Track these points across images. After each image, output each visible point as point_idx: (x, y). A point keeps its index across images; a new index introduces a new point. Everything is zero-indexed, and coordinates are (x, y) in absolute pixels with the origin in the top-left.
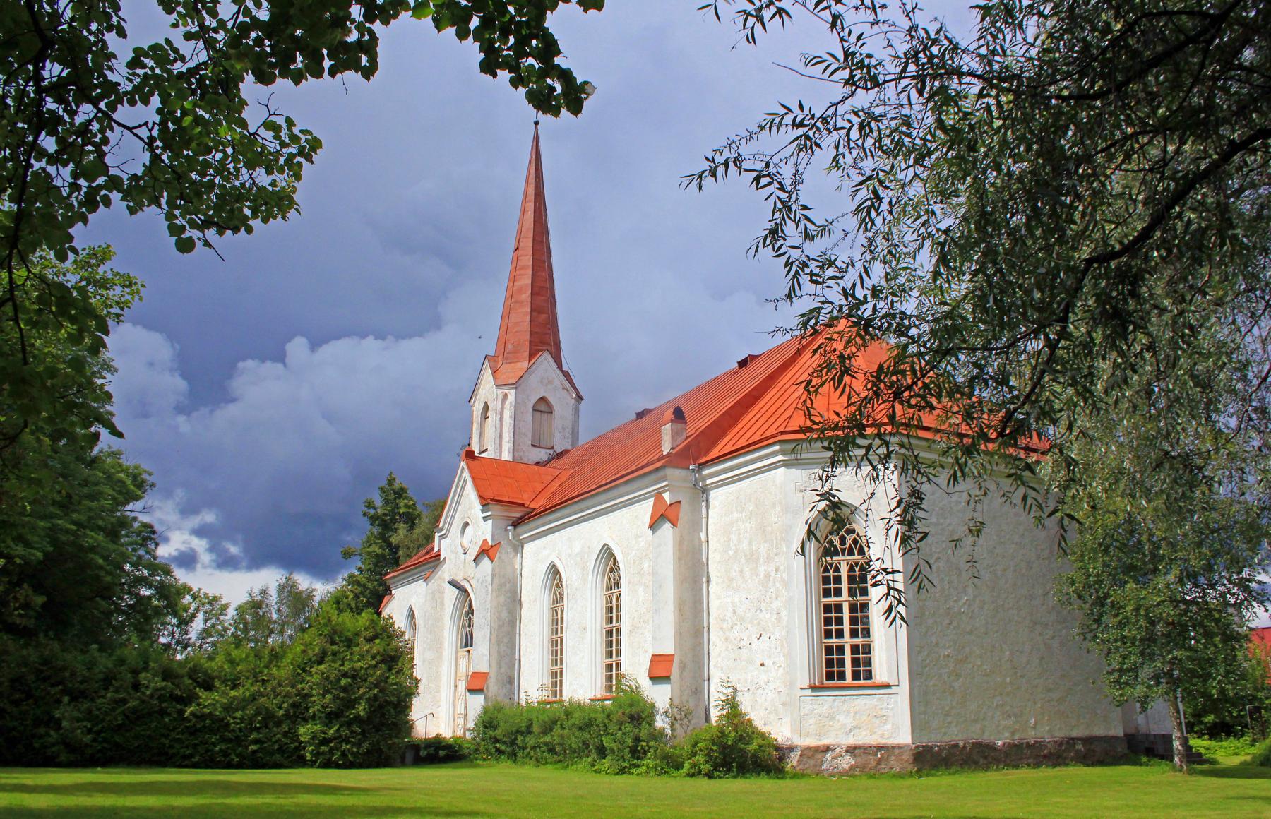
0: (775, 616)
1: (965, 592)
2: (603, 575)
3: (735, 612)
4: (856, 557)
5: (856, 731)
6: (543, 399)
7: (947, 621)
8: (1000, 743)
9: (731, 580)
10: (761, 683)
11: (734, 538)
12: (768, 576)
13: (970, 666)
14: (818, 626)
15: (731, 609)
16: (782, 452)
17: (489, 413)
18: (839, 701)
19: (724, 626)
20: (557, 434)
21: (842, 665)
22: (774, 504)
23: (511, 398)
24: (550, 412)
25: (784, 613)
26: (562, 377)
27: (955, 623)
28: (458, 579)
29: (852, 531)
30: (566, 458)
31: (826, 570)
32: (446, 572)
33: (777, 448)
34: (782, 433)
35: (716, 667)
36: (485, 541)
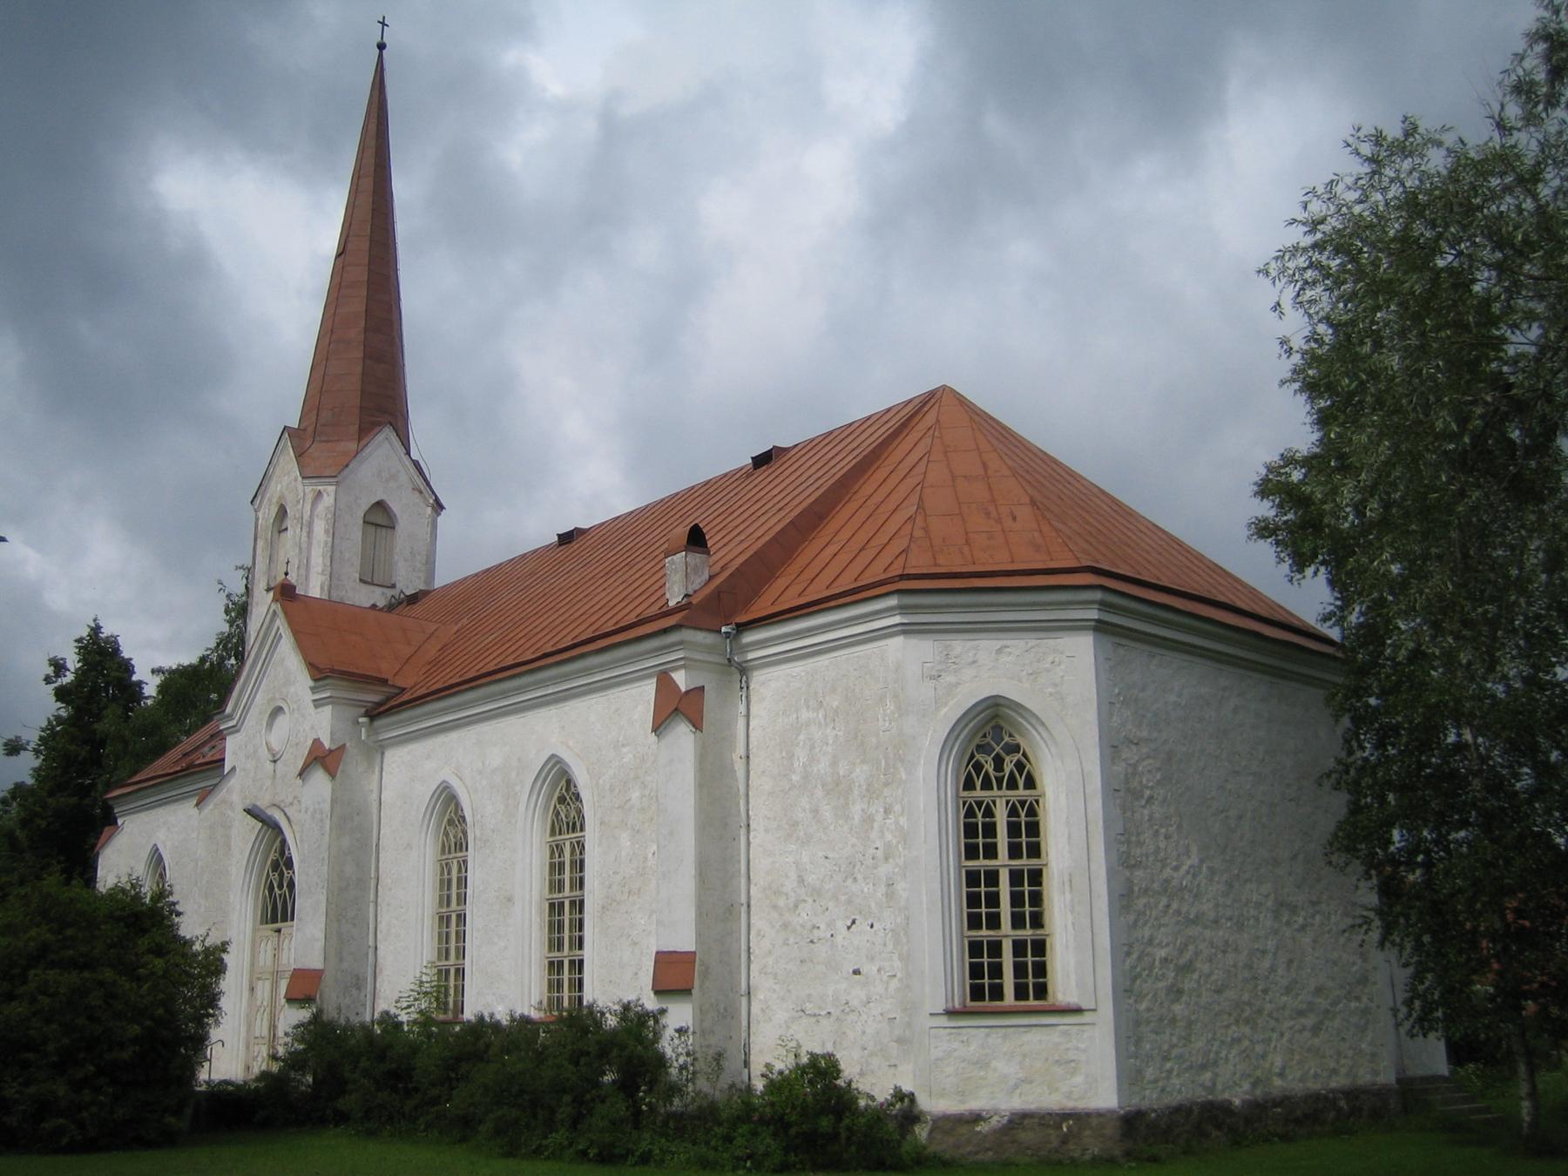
0: (882, 889)
1: (1188, 853)
2: (546, 808)
3: (801, 880)
4: (1021, 792)
6: (380, 506)
7: (1164, 901)
9: (795, 824)
10: (855, 1003)
11: (801, 755)
12: (868, 820)
13: (1196, 976)
14: (957, 909)
15: (793, 875)
16: (903, 609)
17: (288, 523)
18: (995, 1038)
19: (781, 902)
20: (401, 564)
21: (1001, 970)
23: (328, 500)
25: (901, 886)
26: (412, 469)
27: (1175, 905)
28: (263, 803)
29: (1016, 748)
30: (418, 608)
31: (970, 813)
32: (235, 792)
33: (893, 601)
34: (903, 577)
35: (763, 971)
36: (317, 743)
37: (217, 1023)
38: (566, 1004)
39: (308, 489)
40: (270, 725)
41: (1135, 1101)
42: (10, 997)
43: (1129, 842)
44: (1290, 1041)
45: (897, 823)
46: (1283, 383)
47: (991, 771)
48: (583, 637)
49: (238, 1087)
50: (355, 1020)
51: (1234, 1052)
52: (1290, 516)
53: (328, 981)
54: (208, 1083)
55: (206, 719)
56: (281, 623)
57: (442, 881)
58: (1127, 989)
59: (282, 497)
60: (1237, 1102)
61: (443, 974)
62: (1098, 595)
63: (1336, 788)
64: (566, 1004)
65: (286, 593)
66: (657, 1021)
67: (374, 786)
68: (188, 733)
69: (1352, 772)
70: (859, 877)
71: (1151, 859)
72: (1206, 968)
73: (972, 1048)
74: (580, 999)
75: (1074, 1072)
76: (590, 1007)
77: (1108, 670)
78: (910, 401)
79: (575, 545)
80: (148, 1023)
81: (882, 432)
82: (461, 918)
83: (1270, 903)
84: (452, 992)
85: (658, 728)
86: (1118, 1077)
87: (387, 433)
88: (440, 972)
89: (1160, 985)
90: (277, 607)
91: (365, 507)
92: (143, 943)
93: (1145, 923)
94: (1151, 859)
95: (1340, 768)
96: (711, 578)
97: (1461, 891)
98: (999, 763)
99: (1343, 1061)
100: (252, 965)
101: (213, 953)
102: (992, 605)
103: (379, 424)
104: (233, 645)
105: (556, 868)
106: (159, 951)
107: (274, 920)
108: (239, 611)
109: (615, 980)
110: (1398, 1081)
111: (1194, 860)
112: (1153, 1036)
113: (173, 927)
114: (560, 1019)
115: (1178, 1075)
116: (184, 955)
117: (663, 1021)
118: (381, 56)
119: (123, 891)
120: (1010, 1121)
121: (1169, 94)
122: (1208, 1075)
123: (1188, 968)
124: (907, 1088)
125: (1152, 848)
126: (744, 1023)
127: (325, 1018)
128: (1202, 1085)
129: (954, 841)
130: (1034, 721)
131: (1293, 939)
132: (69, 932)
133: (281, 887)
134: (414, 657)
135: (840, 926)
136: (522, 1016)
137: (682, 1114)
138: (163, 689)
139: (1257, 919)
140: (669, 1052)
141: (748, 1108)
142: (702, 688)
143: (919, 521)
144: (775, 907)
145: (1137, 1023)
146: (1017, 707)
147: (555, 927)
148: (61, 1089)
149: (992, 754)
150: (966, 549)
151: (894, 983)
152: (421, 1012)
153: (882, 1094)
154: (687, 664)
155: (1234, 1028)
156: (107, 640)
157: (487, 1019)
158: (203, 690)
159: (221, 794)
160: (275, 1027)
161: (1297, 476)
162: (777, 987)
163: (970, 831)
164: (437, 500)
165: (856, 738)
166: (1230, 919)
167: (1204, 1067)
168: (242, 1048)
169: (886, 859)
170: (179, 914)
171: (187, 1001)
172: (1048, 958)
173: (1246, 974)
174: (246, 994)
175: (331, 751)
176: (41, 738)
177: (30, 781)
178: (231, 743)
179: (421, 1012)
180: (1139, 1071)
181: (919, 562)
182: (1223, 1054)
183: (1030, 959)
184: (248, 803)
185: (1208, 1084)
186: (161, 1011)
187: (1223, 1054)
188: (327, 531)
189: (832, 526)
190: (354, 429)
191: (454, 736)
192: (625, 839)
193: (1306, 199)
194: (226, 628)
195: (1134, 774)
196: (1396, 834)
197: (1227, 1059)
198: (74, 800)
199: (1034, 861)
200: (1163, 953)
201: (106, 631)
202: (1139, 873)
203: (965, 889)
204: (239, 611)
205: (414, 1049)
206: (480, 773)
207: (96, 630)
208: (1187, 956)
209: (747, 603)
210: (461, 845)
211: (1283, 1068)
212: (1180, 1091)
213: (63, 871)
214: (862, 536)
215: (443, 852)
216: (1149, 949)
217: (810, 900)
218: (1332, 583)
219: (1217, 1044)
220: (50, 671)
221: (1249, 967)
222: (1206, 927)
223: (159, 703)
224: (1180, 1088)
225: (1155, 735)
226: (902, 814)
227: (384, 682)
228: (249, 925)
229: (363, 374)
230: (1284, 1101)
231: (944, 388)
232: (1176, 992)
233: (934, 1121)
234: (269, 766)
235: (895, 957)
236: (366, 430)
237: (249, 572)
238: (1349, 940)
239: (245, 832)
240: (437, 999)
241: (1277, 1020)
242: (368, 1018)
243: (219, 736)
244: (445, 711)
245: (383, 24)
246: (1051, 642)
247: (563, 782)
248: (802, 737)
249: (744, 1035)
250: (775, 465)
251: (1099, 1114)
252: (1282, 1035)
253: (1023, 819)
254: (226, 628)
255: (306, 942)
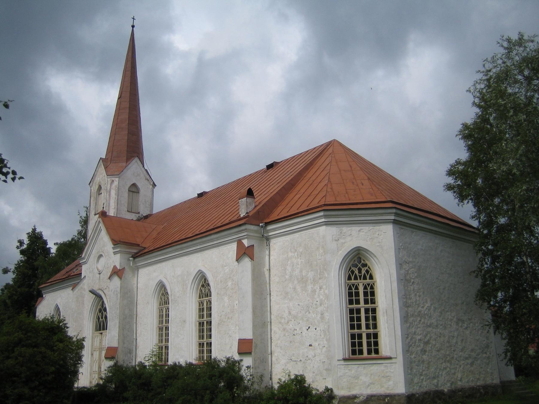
0: (319, 316)
1: (427, 302)
2: (197, 288)
3: (290, 313)
5: (372, 386)
6: (134, 185)
7: (419, 319)
8: (446, 390)
10: (310, 356)
11: (289, 268)
12: (314, 291)
13: (430, 346)
15: (287, 311)
16: (325, 216)
17: (102, 191)
18: (361, 368)
19: (283, 321)
21: (362, 344)
22: (318, 248)
23: (116, 183)
24: (138, 192)
25: (326, 314)
26: (145, 172)
27: (423, 320)
28: (96, 288)
29: (365, 265)
30: (148, 220)
31: (350, 288)
32: (86, 285)
33: (322, 214)
34: (325, 205)
36: (115, 267)
37: (81, 366)
38: (205, 358)
39: (109, 179)
40: (98, 261)
41: (411, 390)
42: (8, 358)
43: (406, 298)
44: (463, 368)
45: (324, 292)
46: (457, 135)
47: (357, 273)
48: (224, 223)
49: (89, 389)
50: (130, 365)
51: (444, 373)
52: (459, 183)
53: (120, 350)
54: (77, 388)
55: (74, 260)
56: (102, 225)
57: (160, 315)
58: (407, 350)
59: (100, 182)
60: (446, 390)
61: (161, 348)
62: (394, 211)
63: (477, 277)
64: (205, 358)
65: (103, 214)
66: (239, 364)
67: (135, 282)
68: (68, 265)
69: (483, 272)
70: (311, 311)
71: (414, 304)
72: (434, 342)
73: (353, 372)
74: (211, 356)
75: (389, 380)
76: (215, 359)
77: (398, 237)
78: (322, 145)
79: (204, 197)
80: (57, 366)
81: (314, 155)
82: (167, 328)
83: (455, 319)
84: (164, 354)
85: (238, 259)
86: (405, 382)
87: (136, 159)
88: (159, 347)
89: (418, 349)
90: (100, 219)
91: (129, 185)
92: (55, 338)
93: (413, 327)
94: (414, 304)
95: (478, 270)
96: (255, 207)
97: (525, 314)
98: (360, 271)
99: (481, 375)
100: (92, 346)
101: (80, 342)
102: (356, 215)
103: (133, 157)
104: (83, 234)
105: (201, 310)
106: (61, 341)
107: (100, 330)
108: (85, 222)
109: (224, 349)
110: (501, 382)
111: (428, 304)
112: (416, 367)
113: (66, 332)
114: (204, 364)
115: (426, 381)
116: (70, 342)
117: (242, 364)
118: (133, 30)
119: (48, 319)
120: (367, 398)
121: (389, 48)
122: (436, 381)
123: (427, 343)
124: (330, 387)
125: (414, 300)
126: (270, 364)
127: (119, 364)
128: (433, 384)
129: (345, 298)
130: (372, 256)
131: (463, 332)
132: (29, 334)
133: (102, 318)
134: (147, 237)
135: (305, 329)
136: (190, 363)
137: (249, 397)
138: (58, 250)
139: (451, 325)
140: (244, 374)
141: (273, 393)
142: (124, 268)
143: (329, 185)
144: (280, 323)
145: (411, 363)
146: (366, 250)
147: (201, 331)
148: (26, 391)
149: (357, 266)
150: (346, 195)
151: (324, 349)
152: (153, 362)
153: (321, 389)
154: (248, 237)
155: (444, 364)
156: (38, 233)
157: (177, 364)
158: (73, 250)
159: (81, 285)
160: (100, 368)
161: (461, 168)
162: (281, 351)
163: (350, 294)
164: (154, 183)
165: (309, 262)
166: (442, 325)
167: (434, 378)
168: (89, 376)
169: (321, 305)
170: (68, 328)
171: (71, 359)
172: (379, 339)
173: (448, 345)
174: (90, 356)
175: (120, 270)
176: (15, 268)
177: (11, 283)
178: (84, 268)
179: (153, 362)
180: (412, 380)
181: (330, 200)
182: (440, 373)
183: (372, 340)
184: (90, 289)
185: (436, 384)
186: (62, 362)
187: (440, 373)
188: (116, 194)
189: (297, 189)
190: (125, 158)
191: (164, 264)
192: (226, 299)
193: (484, 63)
194: (80, 228)
195: (407, 274)
196: (499, 294)
197: (442, 375)
198: (27, 290)
199: (373, 305)
200: (419, 337)
201: (38, 230)
202: (410, 309)
203: (349, 315)
204: (85, 222)
205: (151, 375)
206: (173, 277)
207: (34, 230)
208: (428, 338)
209: (268, 215)
210: (167, 302)
211: (461, 378)
212: (426, 387)
213: (27, 312)
214: (309, 192)
215: (160, 305)
216: (414, 336)
217: (293, 320)
218: (475, 206)
219: (438, 370)
220: (18, 244)
221: (448, 342)
222: (433, 328)
223: (57, 255)
224: (426, 385)
225: (414, 260)
226: (326, 289)
227: (138, 245)
228: (91, 331)
229: (127, 140)
230: (462, 390)
231: (334, 140)
232: (424, 351)
233: (340, 398)
234: (98, 276)
235: (325, 340)
236: (129, 159)
237: (88, 209)
238: (482, 332)
239: (89, 299)
240: (159, 357)
241: (459, 361)
242: (134, 364)
243: (80, 265)
244: (160, 255)
245: (134, 19)
246: (378, 227)
247: (203, 280)
248: (289, 262)
249: (270, 368)
250: (274, 168)
251: (399, 395)
252: (460, 366)
253: (354, 290)
254: (80, 228)
255: (112, 337)
